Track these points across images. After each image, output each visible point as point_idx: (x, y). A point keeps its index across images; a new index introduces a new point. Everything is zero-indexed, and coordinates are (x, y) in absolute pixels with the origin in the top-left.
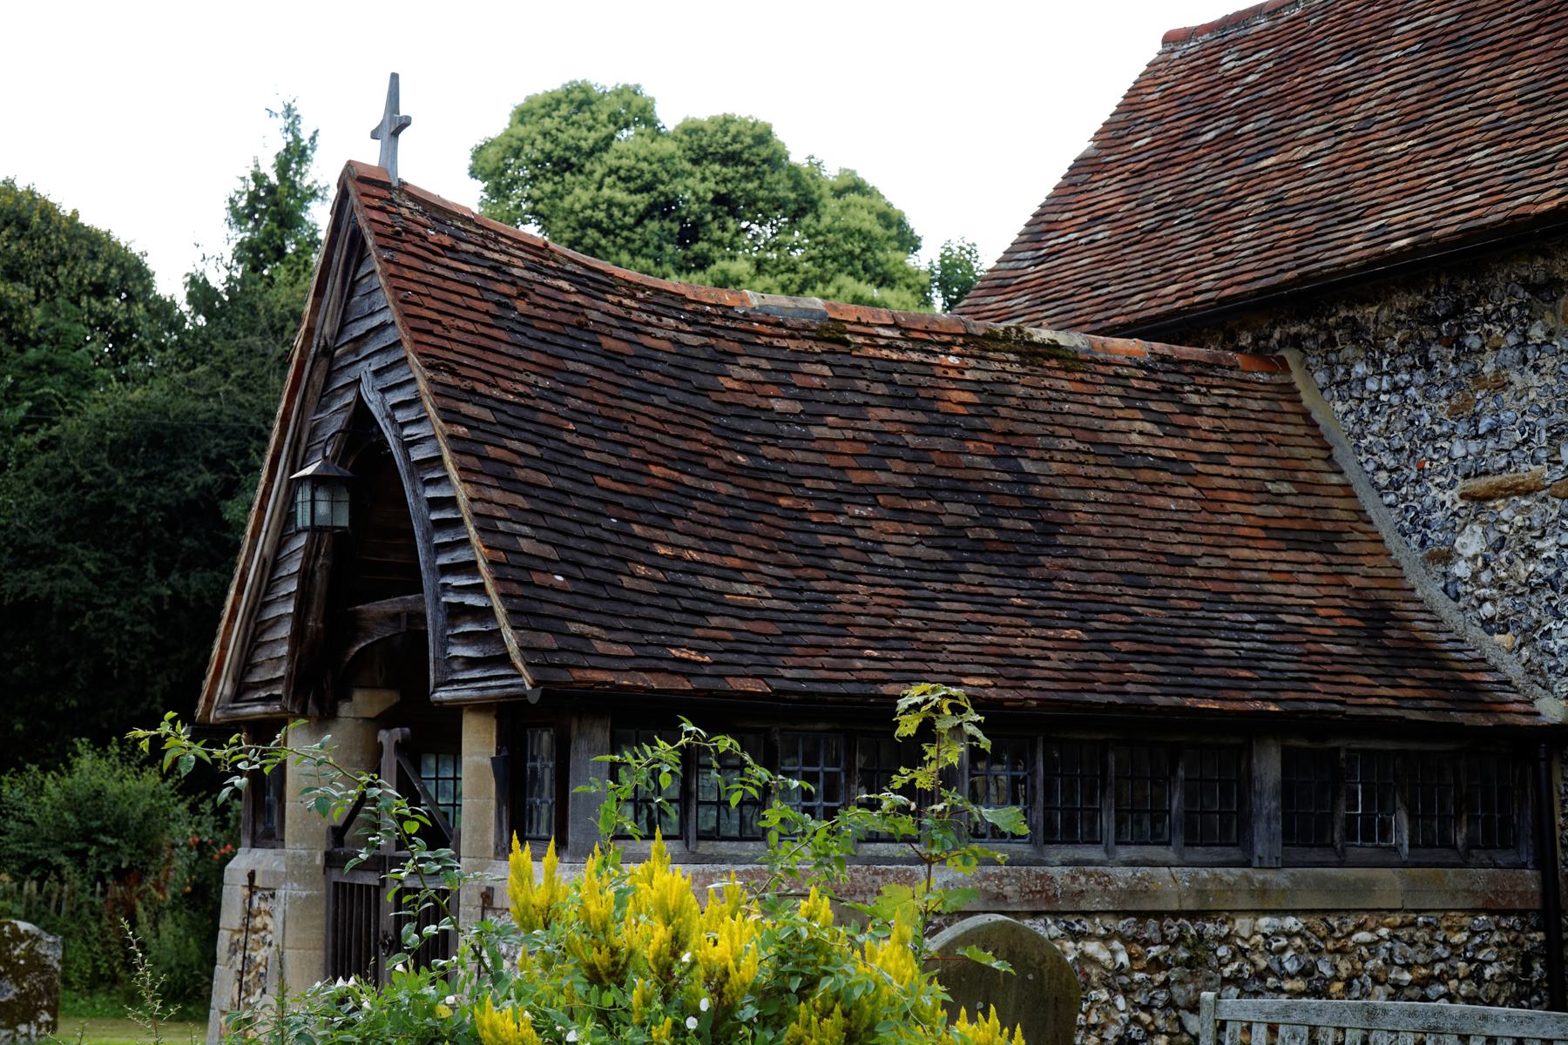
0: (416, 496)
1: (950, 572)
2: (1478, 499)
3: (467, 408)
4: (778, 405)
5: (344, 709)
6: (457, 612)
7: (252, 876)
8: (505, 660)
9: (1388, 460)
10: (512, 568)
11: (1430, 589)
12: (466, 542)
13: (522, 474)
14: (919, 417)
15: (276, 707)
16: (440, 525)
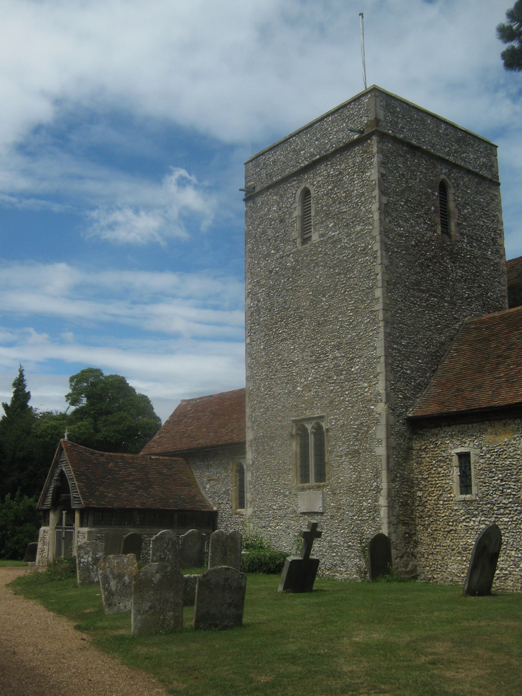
0: (70, 482)
1: (137, 491)
2: (209, 481)
3: (77, 472)
4: (116, 469)
5: (58, 508)
6: (75, 497)
7: (44, 530)
8: (81, 503)
9: (199, 474)
10: (82, 493)
11: (203, 492)
12: (76, 489)
13: (83, 481)
14: (135, 470)
15: (49, 508)
16: (73, 486)
